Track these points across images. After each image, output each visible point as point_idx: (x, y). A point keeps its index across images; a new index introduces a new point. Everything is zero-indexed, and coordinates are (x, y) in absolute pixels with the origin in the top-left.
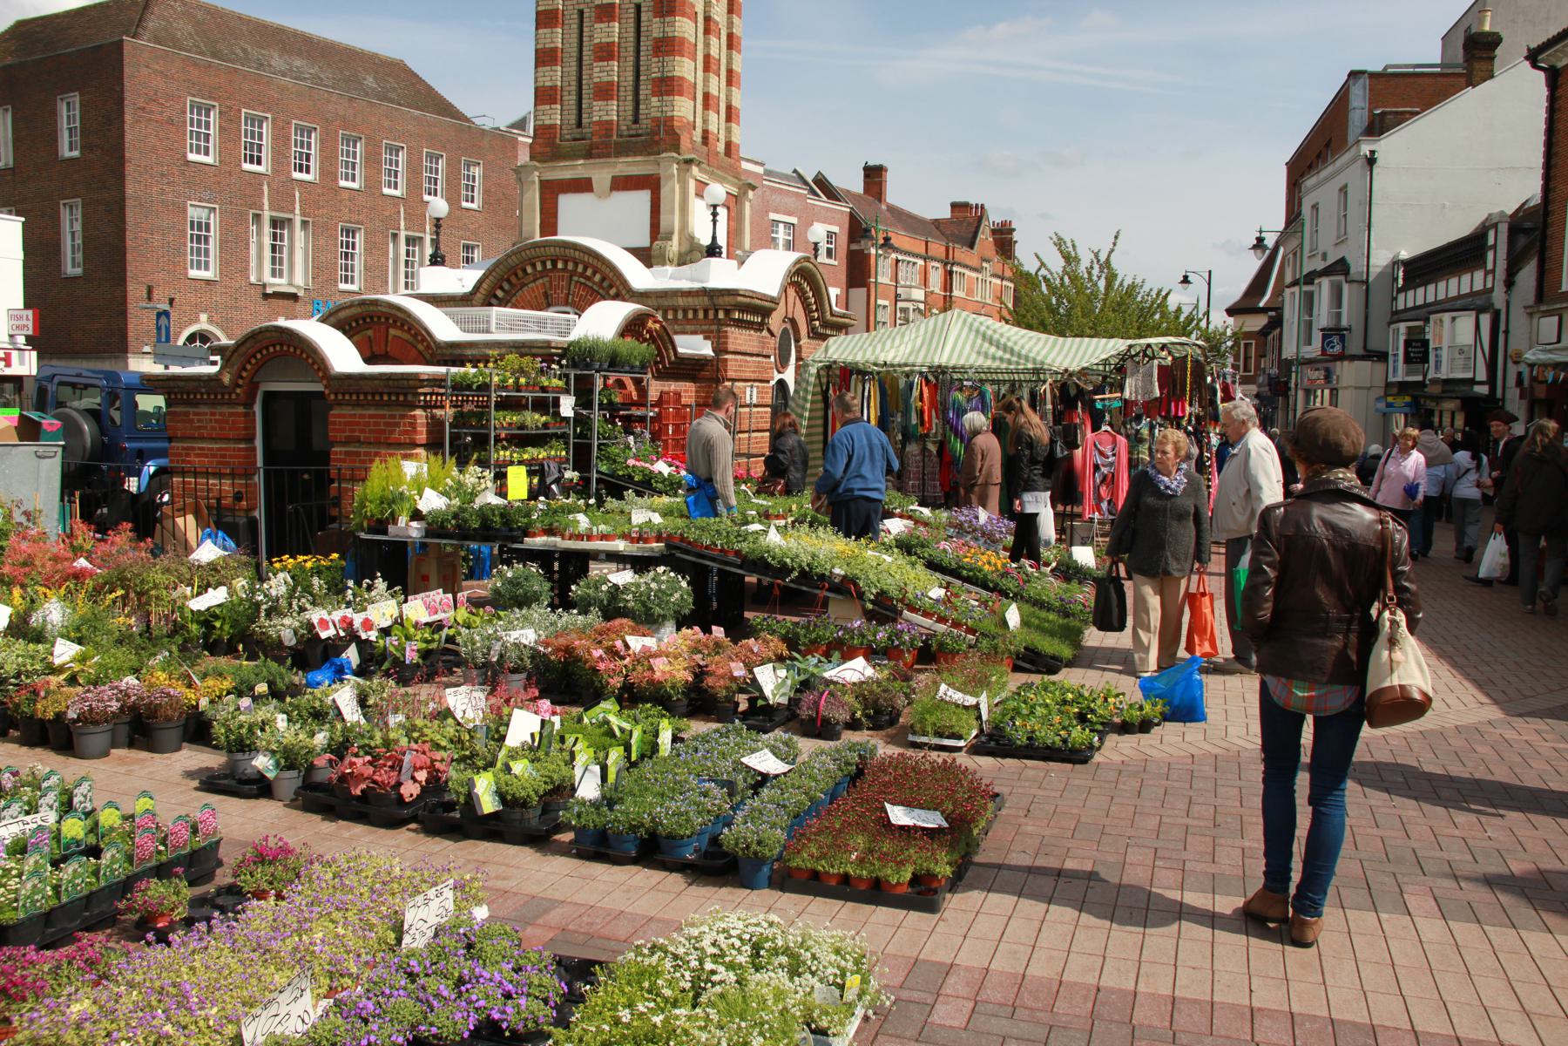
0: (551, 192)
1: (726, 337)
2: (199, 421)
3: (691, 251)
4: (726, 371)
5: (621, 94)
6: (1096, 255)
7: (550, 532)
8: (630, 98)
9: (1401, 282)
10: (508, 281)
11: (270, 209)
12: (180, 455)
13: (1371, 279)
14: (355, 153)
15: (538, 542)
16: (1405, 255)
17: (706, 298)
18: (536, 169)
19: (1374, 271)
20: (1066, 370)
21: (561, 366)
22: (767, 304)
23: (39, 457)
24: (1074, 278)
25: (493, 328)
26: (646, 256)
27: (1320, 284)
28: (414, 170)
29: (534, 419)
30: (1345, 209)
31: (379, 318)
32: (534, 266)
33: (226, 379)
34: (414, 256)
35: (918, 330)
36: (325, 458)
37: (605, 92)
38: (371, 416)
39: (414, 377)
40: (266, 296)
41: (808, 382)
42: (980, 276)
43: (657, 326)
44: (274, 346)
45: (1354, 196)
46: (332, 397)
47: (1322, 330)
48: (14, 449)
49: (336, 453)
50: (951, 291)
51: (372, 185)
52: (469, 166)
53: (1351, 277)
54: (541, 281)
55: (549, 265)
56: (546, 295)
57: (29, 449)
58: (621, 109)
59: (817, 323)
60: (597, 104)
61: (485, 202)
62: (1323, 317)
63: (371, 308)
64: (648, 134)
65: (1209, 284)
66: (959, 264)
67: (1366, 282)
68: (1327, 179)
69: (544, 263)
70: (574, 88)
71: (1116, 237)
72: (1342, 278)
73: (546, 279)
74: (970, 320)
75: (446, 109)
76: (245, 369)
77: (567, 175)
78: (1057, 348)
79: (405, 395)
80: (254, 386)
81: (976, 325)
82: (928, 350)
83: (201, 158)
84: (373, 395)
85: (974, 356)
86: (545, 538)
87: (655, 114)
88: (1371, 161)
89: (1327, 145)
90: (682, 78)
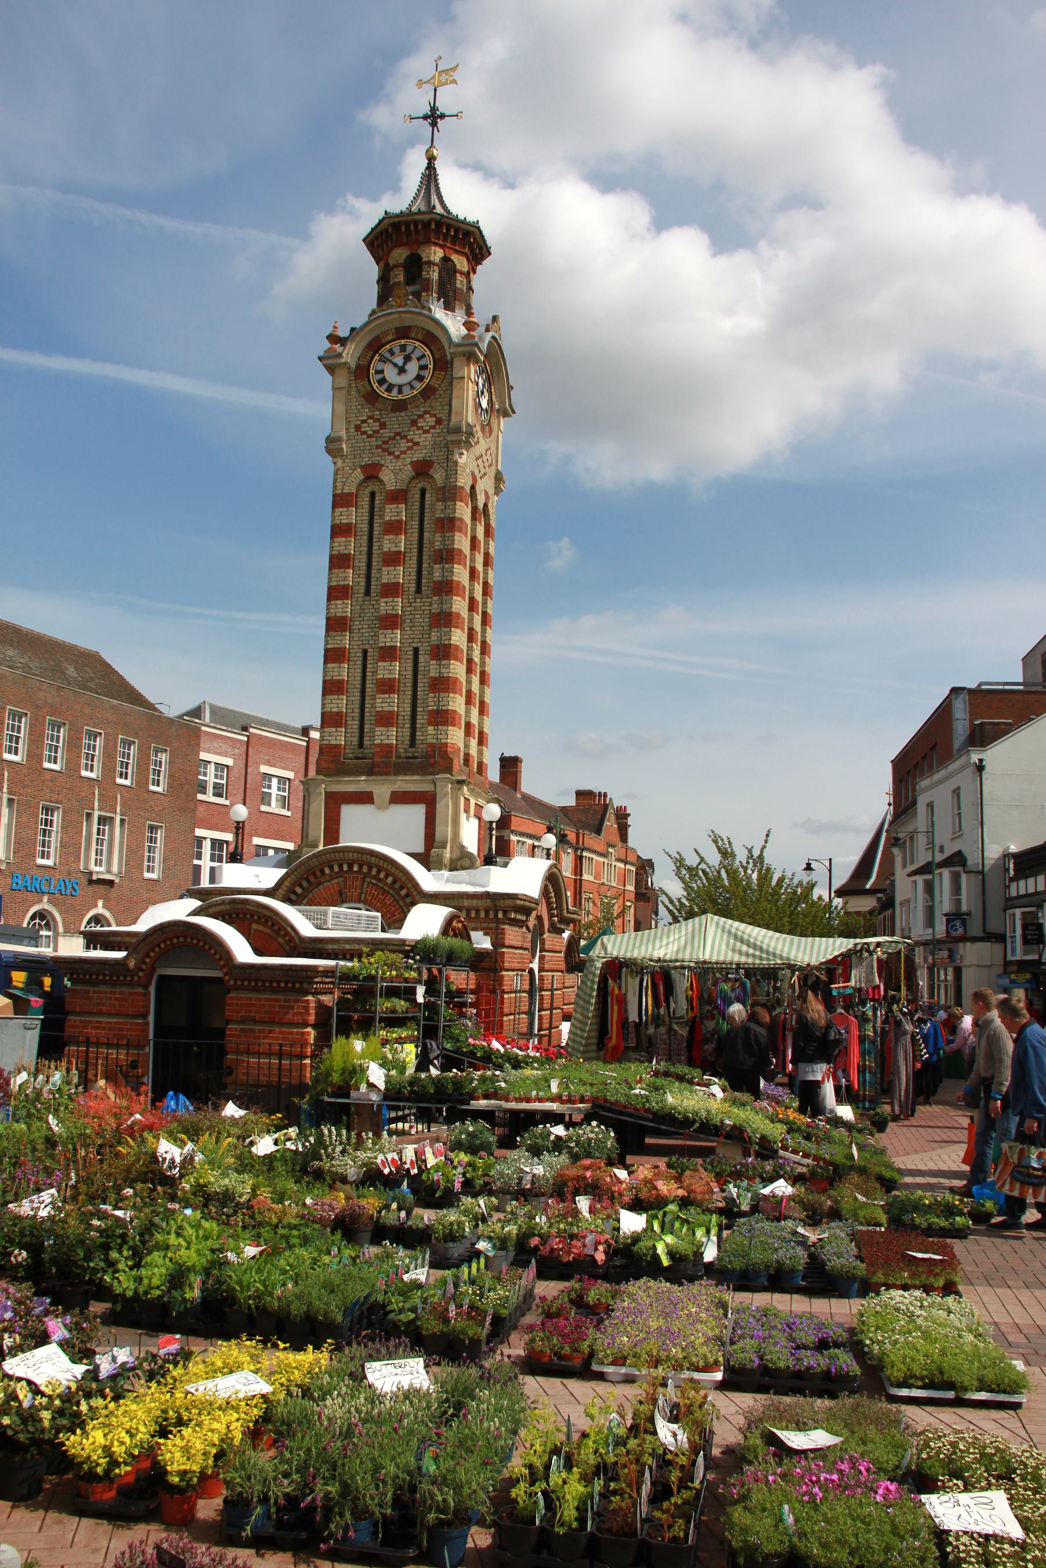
0: (335, 802)
1: (504, 934)
2: (98, 998)
3: (461, 858)
4: (503, 962)
5: (400, 722)
6: (750, 851)
7: (486, 1096)
8: (408, 726)
9: (1012, 872)
10: (307, 880)
11: (100, 810)
12: (77, 1027)
13: (986, 870)
14: (58, 737)
15: (482, 1103)
16: (1013, 849)
17: (489, 901)
18: (323, 782)
19: (988, 863)
20: (808, 965)
21: (416, 961)
22: (527, 904)
23: (26, 1028)
24: (732, 874)
25: (330, 923)
26: (425, 860)
27: (941, 875)
28: (109, 755)
29: (401, 1005)
30: (959, 808)
31: (245, 915)
32: (331, 868)
33: (132, 964)
34: (104, 835)
35: (680, 932)
36: (221, 1033)
37: (386, 719)
38: (266, 1000)
39: (314, 968)
40: (91, 882)
41: (594, 974)
42: (606, 861)
43: (460, 925)
44: (178, 938)
45: (966, 798)
46: (232, 982)
47: (945, 915)
48: (11, 1022)
49: (231, 1030)
50: (581, 875)
51: (72, 767)
52: (157, 752)
53: (968, 868)
54: (336, 881)
55: (345, 868)
56: (340, 893)
57: (21, 1022)
58: (400, 734)
59: (556, 919)
60: (379, 730)
61: (170, 786)
62: (944, 903)
63: (240, 906)
64: (423, 757)
65: (830, 871)
66: (589, 850)
67: (982, 872)
68: (941, 782)
69: (341, 866)
70: (357, 714)
71: (767, 835)
72: (960, 869)
73: (341, 879)
74: (721, 923)
75: (136, 698)
76: (148, 956)
77: (351, 788)
78: (795, 945)
79: (301, 983)
80: (153, 969)
81: (727, 927)
82: (692, 947)
83: (52, 766)
84: (271, 982)
85: (730, 953)
86: (485, 1101)
87: (431, 740)
88: (980, 768)
89: (933, 748)
90: (454, 712)
